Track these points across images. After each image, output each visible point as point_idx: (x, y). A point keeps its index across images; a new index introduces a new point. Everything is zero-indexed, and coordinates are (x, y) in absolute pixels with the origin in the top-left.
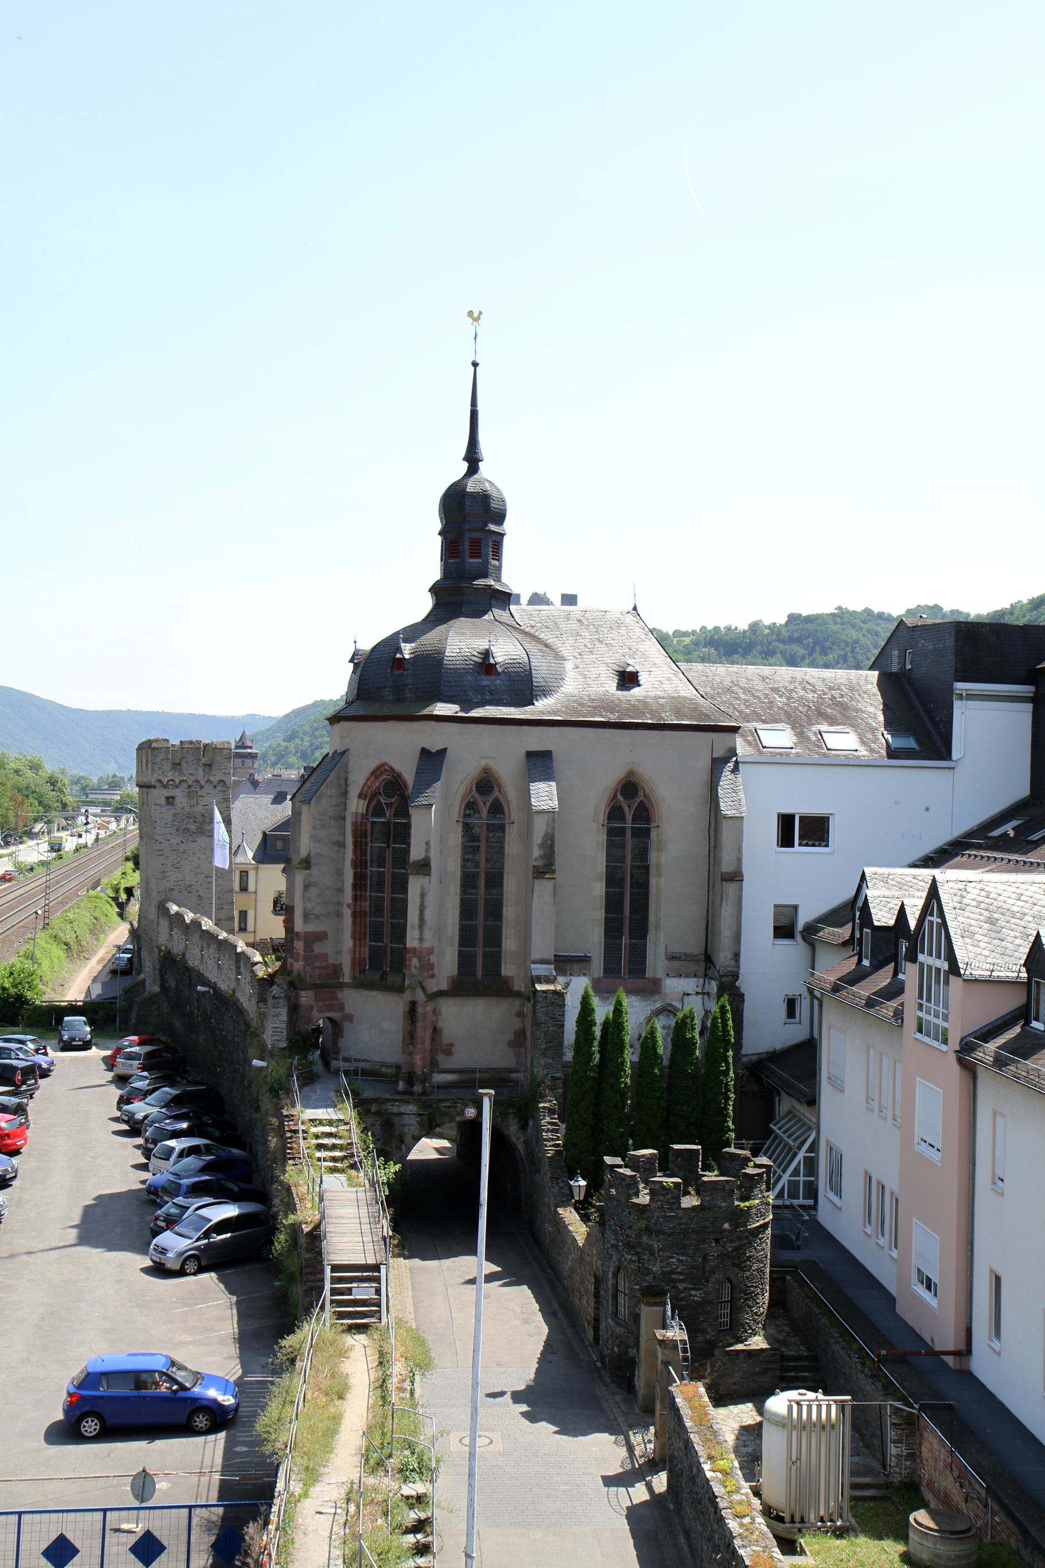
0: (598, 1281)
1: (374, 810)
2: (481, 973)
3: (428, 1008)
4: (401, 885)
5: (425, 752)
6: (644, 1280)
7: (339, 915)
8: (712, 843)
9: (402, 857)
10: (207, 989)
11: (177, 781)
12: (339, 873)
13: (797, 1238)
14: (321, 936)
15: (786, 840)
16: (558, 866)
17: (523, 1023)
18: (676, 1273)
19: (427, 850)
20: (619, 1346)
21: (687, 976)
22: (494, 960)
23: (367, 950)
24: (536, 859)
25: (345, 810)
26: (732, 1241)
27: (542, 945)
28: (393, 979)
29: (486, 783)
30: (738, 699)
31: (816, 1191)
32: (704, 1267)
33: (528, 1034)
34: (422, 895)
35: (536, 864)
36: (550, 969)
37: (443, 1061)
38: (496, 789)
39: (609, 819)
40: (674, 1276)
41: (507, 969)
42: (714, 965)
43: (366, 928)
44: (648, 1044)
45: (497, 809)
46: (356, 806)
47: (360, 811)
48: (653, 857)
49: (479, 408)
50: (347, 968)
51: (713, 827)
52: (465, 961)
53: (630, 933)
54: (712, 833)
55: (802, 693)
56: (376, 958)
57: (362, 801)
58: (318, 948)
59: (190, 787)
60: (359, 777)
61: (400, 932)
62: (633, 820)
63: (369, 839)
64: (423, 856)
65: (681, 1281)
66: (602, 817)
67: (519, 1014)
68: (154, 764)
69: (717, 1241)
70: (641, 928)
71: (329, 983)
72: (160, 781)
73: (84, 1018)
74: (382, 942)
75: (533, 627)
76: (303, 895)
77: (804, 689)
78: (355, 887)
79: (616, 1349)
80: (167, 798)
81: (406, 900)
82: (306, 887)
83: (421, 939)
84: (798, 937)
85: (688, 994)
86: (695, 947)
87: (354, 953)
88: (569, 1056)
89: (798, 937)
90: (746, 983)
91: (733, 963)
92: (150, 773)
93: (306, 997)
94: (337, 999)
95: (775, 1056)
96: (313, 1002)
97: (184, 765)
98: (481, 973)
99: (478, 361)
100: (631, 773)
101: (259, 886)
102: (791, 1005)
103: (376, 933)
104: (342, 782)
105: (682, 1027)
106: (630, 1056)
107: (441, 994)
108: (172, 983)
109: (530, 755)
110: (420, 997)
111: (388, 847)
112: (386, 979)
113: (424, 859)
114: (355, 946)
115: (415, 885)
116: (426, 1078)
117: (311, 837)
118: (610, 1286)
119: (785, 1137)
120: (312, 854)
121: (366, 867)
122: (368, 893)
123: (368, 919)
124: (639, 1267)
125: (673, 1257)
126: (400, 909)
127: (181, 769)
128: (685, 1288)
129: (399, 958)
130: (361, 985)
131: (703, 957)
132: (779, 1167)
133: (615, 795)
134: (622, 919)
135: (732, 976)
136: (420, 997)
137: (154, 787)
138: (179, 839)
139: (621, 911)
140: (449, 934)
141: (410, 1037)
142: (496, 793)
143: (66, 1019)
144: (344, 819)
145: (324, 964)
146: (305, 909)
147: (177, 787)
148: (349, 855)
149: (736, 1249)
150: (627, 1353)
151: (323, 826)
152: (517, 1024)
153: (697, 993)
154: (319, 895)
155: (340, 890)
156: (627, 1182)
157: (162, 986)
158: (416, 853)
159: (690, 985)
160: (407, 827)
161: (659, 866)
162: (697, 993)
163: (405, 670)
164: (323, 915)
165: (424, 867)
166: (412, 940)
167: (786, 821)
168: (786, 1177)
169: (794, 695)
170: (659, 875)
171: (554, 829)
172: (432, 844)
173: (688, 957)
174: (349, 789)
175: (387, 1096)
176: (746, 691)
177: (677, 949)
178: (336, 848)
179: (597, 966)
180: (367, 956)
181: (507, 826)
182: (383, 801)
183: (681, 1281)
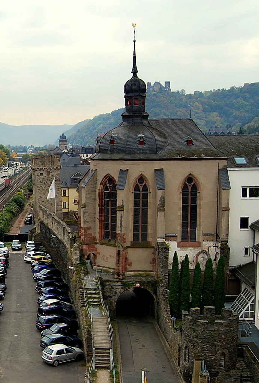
0: (180, 348)
1: (105, 188)
2: (141, 238)
3: (124, 252)
4: (114, 213)
5: (121, 170)
6: (195, 352)
7: (95, 221)
8: (219, 198)
9: (114, 204)
10: (55, 236)
11: (44, 168)
12: (95, 208)
13: (248, 333)
14: (89, 228)
15: (244, 195)
16: (166, 207)
17: (155, 256)
18: (205, 350)
19: (123, 203)
20: (186, 370)
21: (210, 241)
22: (145, 236)
23: (104, 232)
24: (158, 205)
25: (96, 188)
26: (225, 341)
27: (161, 232)
28: (112, 242)
29: (141, 179)
30: (227, 147)
31: (255, 316)
32: (215, 349)
33: (156, 260)
34: (121, 217)
35: (158, 206)
36: (164, 240)
37: (129, 268)
38: (145, 181)
39: (183, 190)
40: (205, 351)
41: (149, 239)
42: (219, 236)
43: (103, 225)
44: (198, 266)
45: (145, 188)
46: (99, 187)
47: (101, 189)
48: (198, 202)
49: (136, 55)
50: (98, 238)
51: (219, 192)
52: (136, 237)
53: (190, 227)
54: (219, 194)
55: (250, 144)
56: (107, 235)
57: (101, 186)
58: (88, 232)
59: (47, 170)
60: (100, 178)
61: (114, 227)
62: (191, 190)
63: (104, 198)
64: (121, 204)
65: (207, 353)
66: (181, 190)
67: (153, 253)
68: (36, 163)
69: (220, 341)
70: (194, 225)
71: (92, 243)
72: (38, 168)
73: (18, 241)
74: (109, 190)
75: (156, 126)
76: (84, 216)
77: (251, 142)
78: (99, 213)
79: (185, 371)
80: (41, 174)
81: (116, 217)
82: (84, 213)
83: (121, 231)
84: (249, 228)
85: (210, 247)
86: (214, 232)
87: (100, 233)
88: (170, 267)
89: (249, 228)
90: (231, 244)
91: (226, 237)
92: (35, 166)
93: (85, 247)
94: (95, 247)
95: (240, 267)
96: (87, 248)
97: (45, 163)
98: (141, 238)
99: (135, 40)
100: (190, 174)
101: (69, 194)
102: (246, 250)
103: (107, 226)
104: (95, 179)
105: (209, 261)
106: (192, 267)
107: (128, 247)
108: (43, 231)
109: (155, 170)
110: (121, 249)
111: (110, 200)
112: (110, 242)
113: (121, 206)
114: (100, 231)
115: (118, 214)
116: (124, 274)
117: (85, 197)
118: (184, 351)
119: (246, 299)
120: (86, 203)
121: (103, 207)
122: (104, 215)
123: (104, 223)
124: (193, 348)
125: (205, 345)
126: (114, 220)
127: (45, 165)
128: (209, 355)
129: (114, 236)
130: (101, 244)
131: (215, 235)
132: (242, 307)
133: (185, 182)
134: (188, 222)
135: (226, 242)
136: (121, 249)
137: (37, 170)
138: (45, 186)
139: (188, 220)
140: (130, 228)
141: (118, 261)
142: (145, 183)
143: (13, 241)
144: (96, 191)
145: (90, 237)
146: (84, 220)
147: (44, 170)
148: (98, 203)
149: (226, 343)
150: (189, 373)
151: (89, 194)
152: (153, 256)
153: (214, 247)
154: (88, 216)
155: (95, 214)
156: (189, 321)
157: (41, 231)
158: (119, 204)
159: (211, 244)
160: (116, 194)
161: (200, 205)
162: (214, 247)
163: (114, 143)
164: (89, 222)
165: (122, 208)
166: (118, 231)
167: (244, 190)
168: (244, 311)
169: (247, 145)
170: (200, 208)
171: (164, 195)
172: (124, 201)
173: (210, 235)
174: (97, 182)
175: (112, 280)
176: (230, 144)
177: (206, 232)
178: (93, 200)
179: (179, 238)
180: (104, 234)
181: (149, 193)
182: (108, 186)
183: (207, 353)
